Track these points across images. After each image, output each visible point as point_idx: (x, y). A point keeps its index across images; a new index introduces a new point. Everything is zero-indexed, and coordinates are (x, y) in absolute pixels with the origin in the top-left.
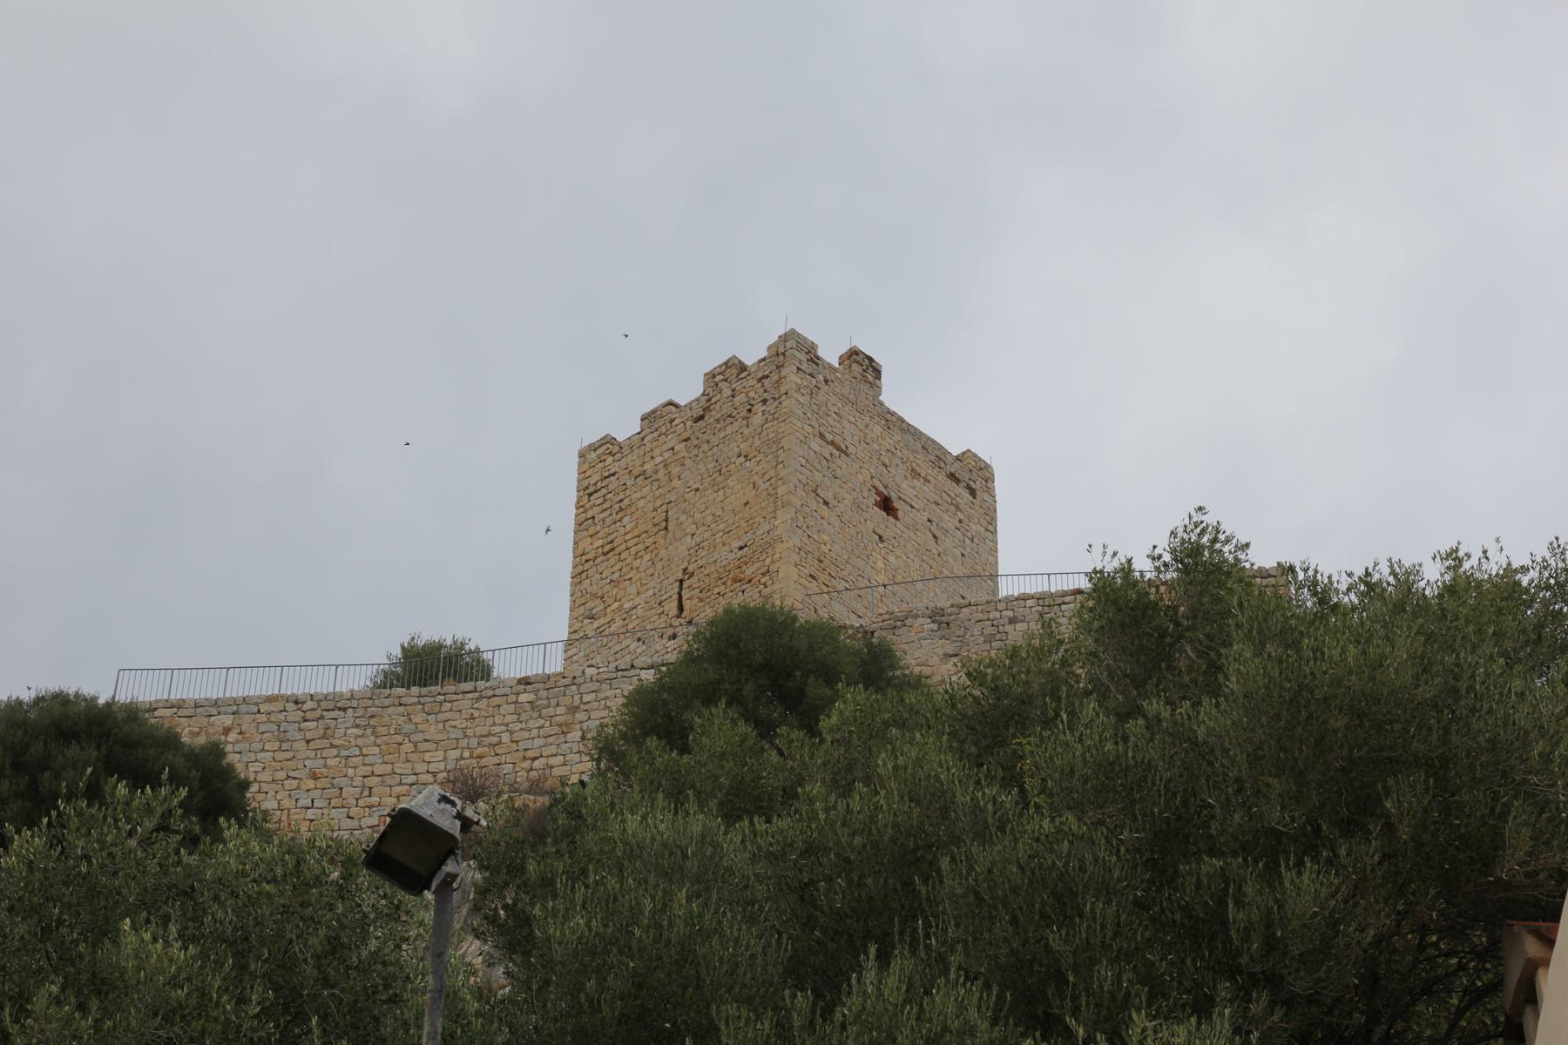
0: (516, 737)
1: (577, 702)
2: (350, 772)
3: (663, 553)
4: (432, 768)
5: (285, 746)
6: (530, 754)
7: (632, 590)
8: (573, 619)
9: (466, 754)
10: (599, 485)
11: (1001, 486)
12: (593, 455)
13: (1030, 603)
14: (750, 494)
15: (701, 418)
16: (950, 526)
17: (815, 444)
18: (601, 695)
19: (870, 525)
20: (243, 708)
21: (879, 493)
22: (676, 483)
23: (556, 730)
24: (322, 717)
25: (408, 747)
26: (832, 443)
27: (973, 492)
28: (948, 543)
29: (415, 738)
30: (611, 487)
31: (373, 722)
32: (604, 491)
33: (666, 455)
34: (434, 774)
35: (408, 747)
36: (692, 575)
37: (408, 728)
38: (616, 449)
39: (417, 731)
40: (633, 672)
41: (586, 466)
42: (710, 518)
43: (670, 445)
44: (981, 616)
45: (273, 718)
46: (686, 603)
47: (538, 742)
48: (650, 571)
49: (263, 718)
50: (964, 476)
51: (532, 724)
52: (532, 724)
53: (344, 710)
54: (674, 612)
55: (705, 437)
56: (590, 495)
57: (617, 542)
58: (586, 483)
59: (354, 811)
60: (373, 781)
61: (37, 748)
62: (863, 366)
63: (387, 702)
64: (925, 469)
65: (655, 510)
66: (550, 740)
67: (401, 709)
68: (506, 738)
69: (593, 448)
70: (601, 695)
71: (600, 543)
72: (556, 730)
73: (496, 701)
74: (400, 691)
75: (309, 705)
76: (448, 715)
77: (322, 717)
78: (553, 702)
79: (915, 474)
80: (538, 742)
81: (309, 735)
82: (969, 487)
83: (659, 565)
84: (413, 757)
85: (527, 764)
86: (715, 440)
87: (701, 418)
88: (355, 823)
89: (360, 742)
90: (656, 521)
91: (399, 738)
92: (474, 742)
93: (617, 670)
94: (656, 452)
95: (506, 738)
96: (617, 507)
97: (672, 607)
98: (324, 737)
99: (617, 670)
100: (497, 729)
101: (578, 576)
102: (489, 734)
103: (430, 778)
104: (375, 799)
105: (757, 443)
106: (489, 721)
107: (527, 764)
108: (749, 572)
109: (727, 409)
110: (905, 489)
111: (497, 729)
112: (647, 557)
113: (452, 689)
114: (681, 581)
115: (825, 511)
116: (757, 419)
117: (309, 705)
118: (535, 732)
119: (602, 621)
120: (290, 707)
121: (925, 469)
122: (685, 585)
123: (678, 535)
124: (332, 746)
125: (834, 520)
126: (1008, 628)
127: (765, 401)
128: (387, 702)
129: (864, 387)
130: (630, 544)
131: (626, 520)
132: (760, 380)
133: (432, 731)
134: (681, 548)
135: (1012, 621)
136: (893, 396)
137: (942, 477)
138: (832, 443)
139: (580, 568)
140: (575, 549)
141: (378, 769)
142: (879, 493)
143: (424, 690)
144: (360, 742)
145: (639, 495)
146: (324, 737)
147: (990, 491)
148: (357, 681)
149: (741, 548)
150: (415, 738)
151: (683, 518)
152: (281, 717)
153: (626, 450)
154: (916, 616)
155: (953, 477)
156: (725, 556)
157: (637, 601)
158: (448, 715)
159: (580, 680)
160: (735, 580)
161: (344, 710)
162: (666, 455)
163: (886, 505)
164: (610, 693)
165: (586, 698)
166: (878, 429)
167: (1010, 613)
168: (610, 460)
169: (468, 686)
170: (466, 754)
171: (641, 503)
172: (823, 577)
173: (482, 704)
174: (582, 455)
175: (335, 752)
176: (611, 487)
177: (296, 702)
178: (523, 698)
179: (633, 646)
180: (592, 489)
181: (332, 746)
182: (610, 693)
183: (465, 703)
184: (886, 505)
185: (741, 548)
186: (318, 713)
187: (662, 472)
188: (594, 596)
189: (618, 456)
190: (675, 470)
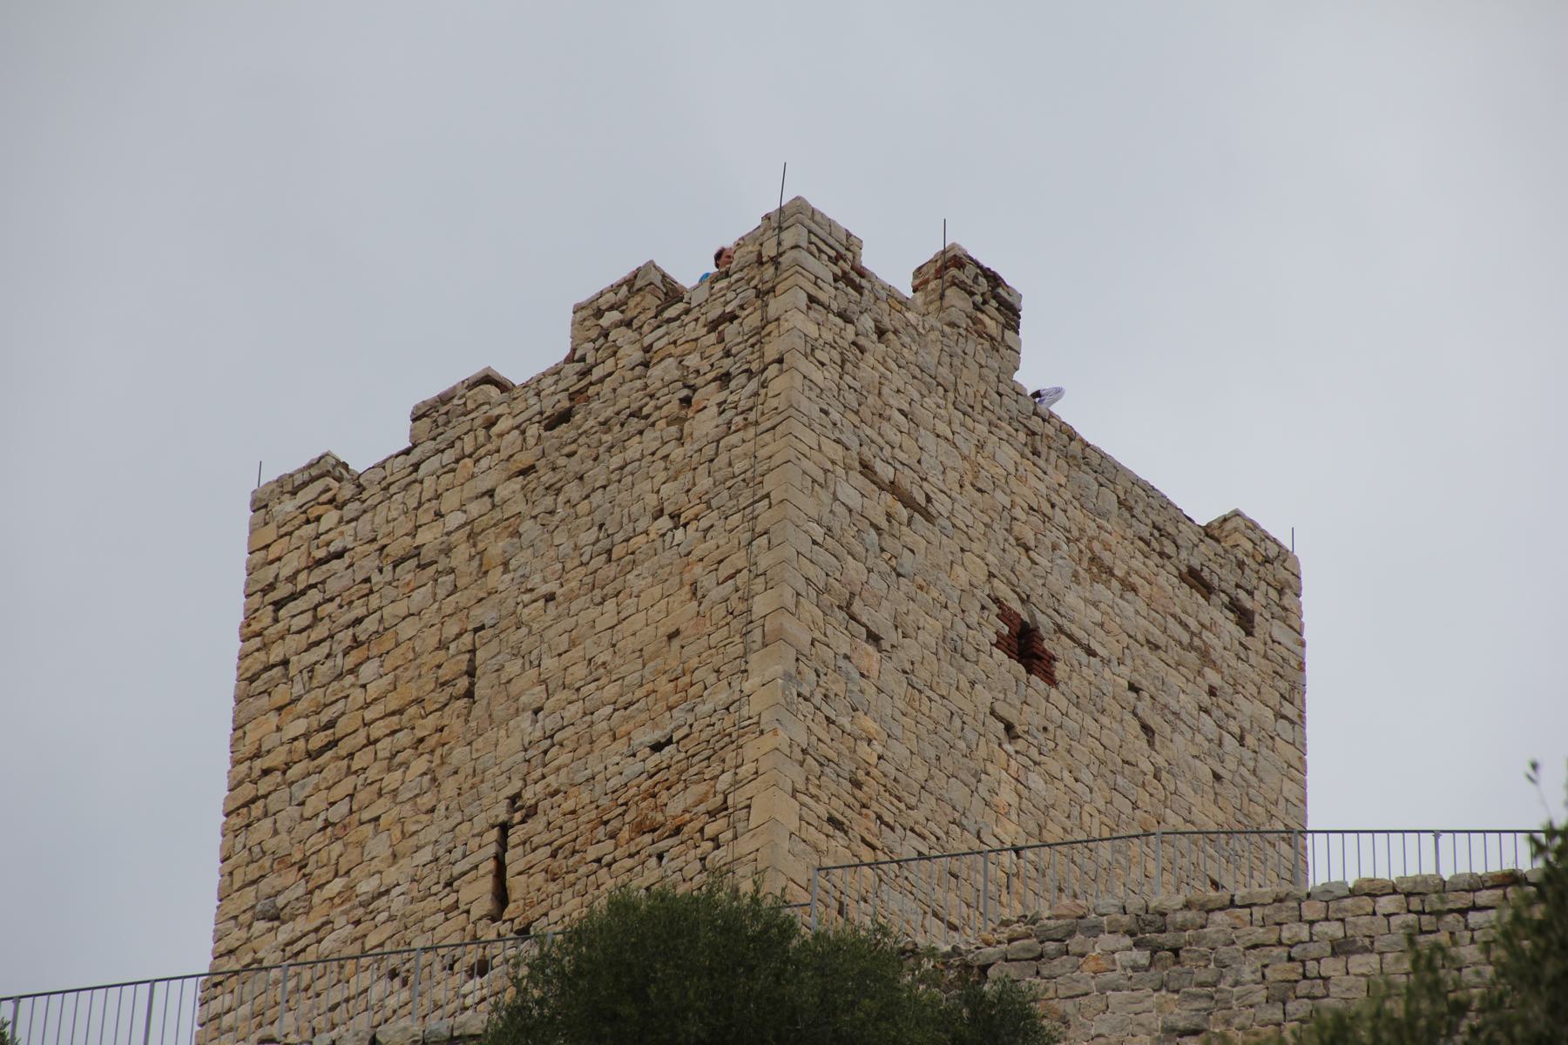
3: (459, 754)
7: (379, 847)
8: (227, 918)
12: (289, 506)
13: (1386, 904)
14: (683, 612)
15: (565, 417)
16: (1187, 704)
17: (851, 490)
19: (984, 696)
21: (1006, 615)
22: (496, 578)
26: (893, 488)
27: (1245, 619)
28: (1179, 746)
30: (333, 587)
32: (314, 596)
33: (474, 508)
36: (531, 812)
38: (348, 490)
41: (270, 533)
43: (484, 484)
44: (1259, 934)
48: (426, 801)
50: (1225, 577)
54: (485, 904)
55: (574, 465)
56: (278, 605)
57: (342, 727)
58: (269, 574)
64: (1125, 557)
65: (442, 646)
69: (289, 486)
71: (300, 726)
79: (1101, 569)
82: (1235, 606)
86: (597, 475)
87: (565, 417)
90: (445, 673)
96: (345, 637)
97: (479, 893)
101: (243, 811)
105: (705, 483)
108: (675, 807)
112: (419, 765)
114: (504, 828)
116: (705, 424)
119: (301, 925)
121: (1125, 557)
123: (499, 711)
125: (899, 687)
126: (1331, 967)
127: (725, 379)
130: (378, 730)
131: (367, 671)
132: (713, 326)
135: (1341, 948)
137: (1167, 580)
138: (893, 488)
139: (247, 791)
142: (1006, 615)
145: (401, 608)
147: (1290, 617)
149: (657, 747)
151: (513, 667)
153: (373, 494)
154: (1095, 930)
155: (1195, 579)
156: (616, 765)
160: (641, 829)
162: (474, 508)
163: (1025, 646)
167: (1335, 930)
168: (331, 517)
171: (407, 629)
176: (333, 587)
180: (283, 590)
184: (1025, 646)
185: (657, 747)
187: (462, 552)
188: (282, 861)
189: (352, 509)
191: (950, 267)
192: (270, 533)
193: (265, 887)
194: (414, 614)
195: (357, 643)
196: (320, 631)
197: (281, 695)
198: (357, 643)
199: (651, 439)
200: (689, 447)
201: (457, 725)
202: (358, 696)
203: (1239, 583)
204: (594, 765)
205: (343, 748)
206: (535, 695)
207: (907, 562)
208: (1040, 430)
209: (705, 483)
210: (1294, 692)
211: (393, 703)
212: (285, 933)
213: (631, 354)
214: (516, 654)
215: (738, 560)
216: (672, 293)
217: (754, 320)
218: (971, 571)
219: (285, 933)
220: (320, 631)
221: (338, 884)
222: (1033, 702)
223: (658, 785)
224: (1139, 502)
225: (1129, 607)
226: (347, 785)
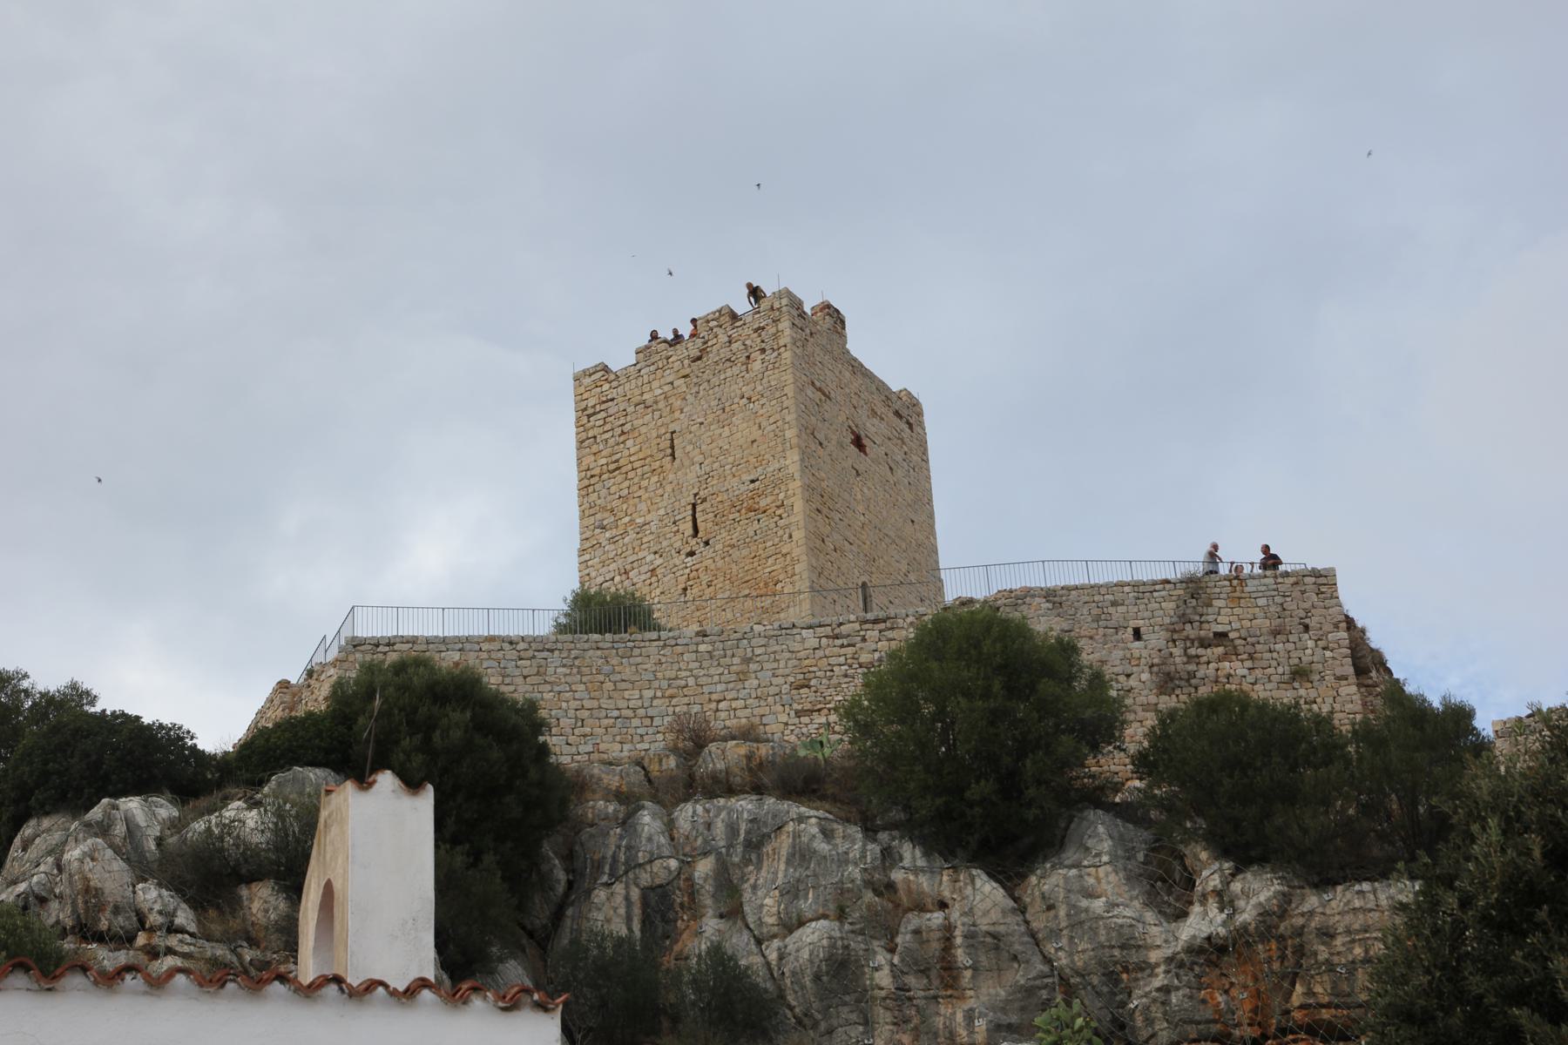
0: (703, 680)
1: (749, 655)
2: (564, 705)
3: (671, 477)
4: (632, 704)
5: (507, 680)
6: (714, 697)
7: (643, 507)
8: (584, 528)
9: (659, 694)
10: (598, 408)
11: (928, 419)
12: (587, 381)
13: (1127, 589)
14: (757, 434)
15: (699, 358)
16: (899, 458)
17: (810, 391)
18: (770, 650)
19: (850, 461)
20: (468, 646)
21: (853, 432)
22: (677, 414)
23: (734, 677)
24: (534, 657)
25: (609, 686)
26: (820, 389)
27: (910, 426)
28: (899, 473)
29: (613, 678)
30: (611, 411)
31: (577, 662)
32: (603, 414)
33: (666, 388)
34: (634, 710)
35: (609, 686)
36: (704, 500)
37: (606, 668)
38: (612, 377)
39: (613, 672)
40: (795, 631)
41: (582, 390)
42: (717, 451)
43: (670, 379)
44: (1087, 599)
45: (493, 655)
46: (701, 526)
47: (720, 687)
48: (660, 491)
49: (485, 655)
50: (904, 412)
51: (712, 671)
52: (712, 671)
53: (552, 651)
54: (690, 531)
55: (705, 376)
56: (589, 416)
57: (622, 462)
58: (583, 405)
59: (571, 739)
60: (586, 714)
61: (423, 711)
62: (834, 317)
63: (586, 646)
64: (881, 409)
65: (659, 437)
66: (731, 686)
67: (599, 653)
68: (691, 681)
69: (587, 373)
70: (770, 650)
71: (604, 461)
72: (734, 677)
73: (679, 649)
74: (596, 637)
75: (521, 646)
76: (639, 660)
77: (534, 657)
78: (729, 653)
79: (874, 413)
80: (720, 687)
81: (525, 672)
82: (908, 423)
83: (669, 488)
84: (615, 694)
85: (713, 706)
86: (715, 381)
87: (699, 358)
88: (574, 750)
89: (569, 679)
90: (662, 446)
91: (601, 678)
92: (665, 684)
93: (781, 628)
94: (655, 384)
95: (691, 681)
96: (618, 431)
97: (687, 527)
98: (538, 674)
99: (781, 628)
100: (684, 674)
101: (585, 489)
102: (676, 678)
103: (629, 713)
104: (587, 730)
105: (759, 388)
106: (676, 666)
107: (713, 706)
108: (763, 503)
109: (725, 353)
110: (873, 429)
111: (684, 674)
112: (655, 479)
113: (639, 637)
114: (694, 506)
115: (820, 451)
116: (757, 366)
117: (521, 646)
118: (716, 678)
119: (614, 532)
120: (506, 646)
121: (881, 409)
122: (699, 509)
123: (687, 463)
124: (546, 682)
125: (827, 459)
126: (1111, 610)
127: (763, 351)
128: (586, 646)
129: (835, 337)
130: (636, 465)
131: (629, 443)
132: (756, 331)
133: (628, 673)
134: (691, 476)
135: (1114, 604)
136: (858, 344)
137: (891, 415)
138: (820, 389)
139: (586, 482)
140: (579, 465)
141: (587, 704)
142: (853, 432)
143: (617, 637)
144: (569, 679)
145: (640, 422)
146: (538, 674)
147: (921, 424)
148: (543, 627)
149: (753, 481)
150: (613, 678)
151: (690, 448)
152: (500, 655)
153: (623, 380)
154: (1033, 596)
155: (897, 414)
156: (738, 486)
157: (649, 518)
158: (639, 660)
159: (750, 635)
160: (750, 510)
161: (552, 651)
162: (666, 388)
163: (858, 443)
164: (777, 648)
165: (758, 651)
166: (847, 374)
167: (1110, 597)
168: (606, 387)
169: (654, 635)
170: (659, 694)
171: (643, 430)
172: (825, 511)
173: (668, 651)
174: (576, 379)
175: (548, 687)
176: (611, 411)
177: (511, 643)
178: (702, 648)
179: (648, 559)
180: (590, 411)
181: (546, 682)
182: (777, 648)
183: (653, 649)
184: (858, 443)
185: (753, 481)
186: (530, 653)
187: (661, 405)
188: (604, 509)
189: (615, 384)
190: (678, 403)
191: (828, 309)
192: (582, 390)
193: (598, 516)
194: (648, 426)
195: (623, 433)
196: (608, 427)
197: (595, 448)
198: (623, 433)
199: (736, 370)
200: (752, 374)
201: (668, 466)
202: (626, 453)
203: (1322, 582)
204: (727, 486)
205: (624, 470)
206: (699, 458)
207: (827, 416)
208: (857, 368)
209: (759, 388)
210: (925, 452)
211: (641, 455)
212: (608, 535)
213: (723, 338)
214: (691, 443)
215: (777, 417)
216: (734, 317)
217: (773, 330)
218: (842, 418)
219: (608, 535)
220: (608, 427)
221: (627, 519)
222: (863, 463)
223: (756, 495)
224: (881, 387)
225: (883, 426)
226: (627, 483)
